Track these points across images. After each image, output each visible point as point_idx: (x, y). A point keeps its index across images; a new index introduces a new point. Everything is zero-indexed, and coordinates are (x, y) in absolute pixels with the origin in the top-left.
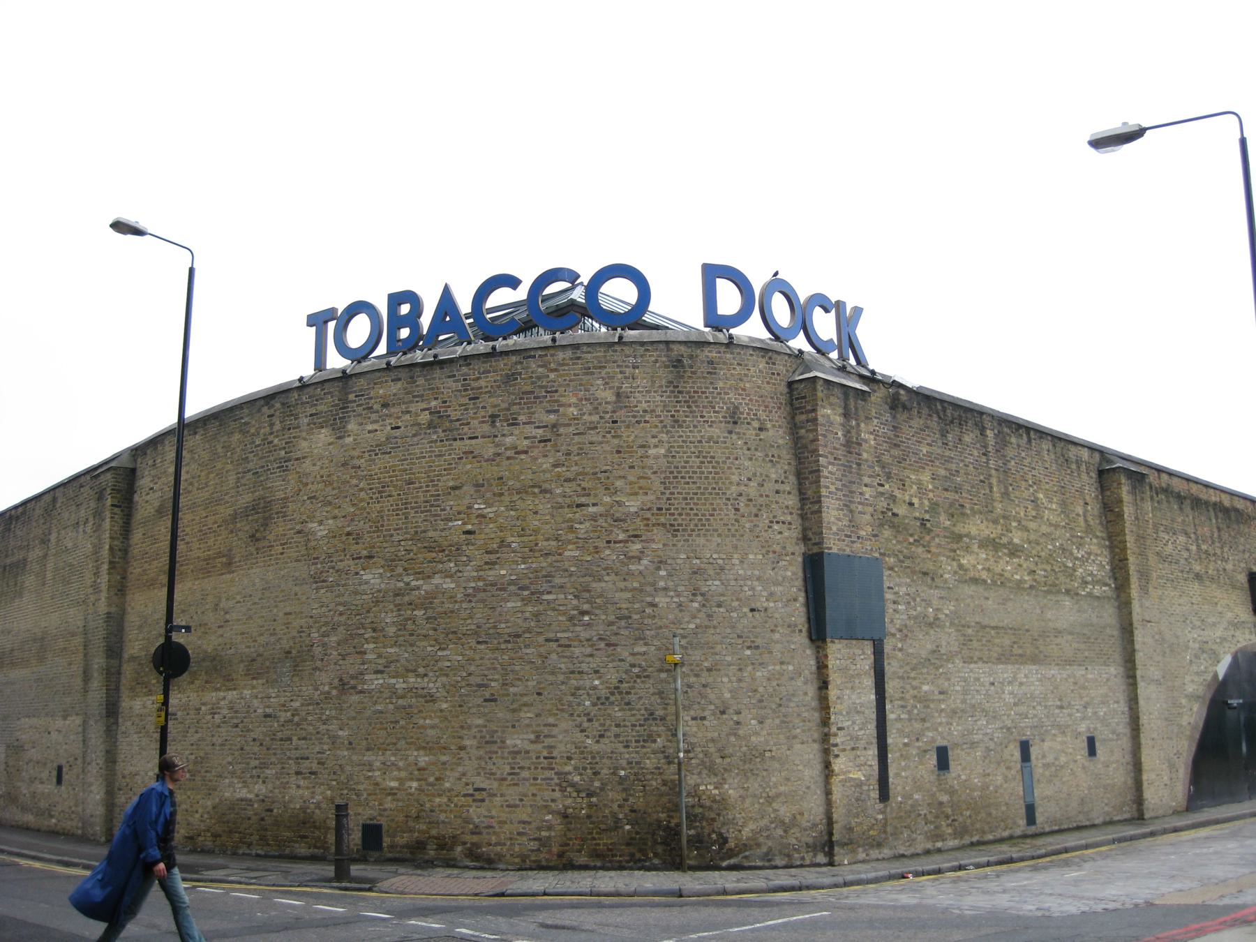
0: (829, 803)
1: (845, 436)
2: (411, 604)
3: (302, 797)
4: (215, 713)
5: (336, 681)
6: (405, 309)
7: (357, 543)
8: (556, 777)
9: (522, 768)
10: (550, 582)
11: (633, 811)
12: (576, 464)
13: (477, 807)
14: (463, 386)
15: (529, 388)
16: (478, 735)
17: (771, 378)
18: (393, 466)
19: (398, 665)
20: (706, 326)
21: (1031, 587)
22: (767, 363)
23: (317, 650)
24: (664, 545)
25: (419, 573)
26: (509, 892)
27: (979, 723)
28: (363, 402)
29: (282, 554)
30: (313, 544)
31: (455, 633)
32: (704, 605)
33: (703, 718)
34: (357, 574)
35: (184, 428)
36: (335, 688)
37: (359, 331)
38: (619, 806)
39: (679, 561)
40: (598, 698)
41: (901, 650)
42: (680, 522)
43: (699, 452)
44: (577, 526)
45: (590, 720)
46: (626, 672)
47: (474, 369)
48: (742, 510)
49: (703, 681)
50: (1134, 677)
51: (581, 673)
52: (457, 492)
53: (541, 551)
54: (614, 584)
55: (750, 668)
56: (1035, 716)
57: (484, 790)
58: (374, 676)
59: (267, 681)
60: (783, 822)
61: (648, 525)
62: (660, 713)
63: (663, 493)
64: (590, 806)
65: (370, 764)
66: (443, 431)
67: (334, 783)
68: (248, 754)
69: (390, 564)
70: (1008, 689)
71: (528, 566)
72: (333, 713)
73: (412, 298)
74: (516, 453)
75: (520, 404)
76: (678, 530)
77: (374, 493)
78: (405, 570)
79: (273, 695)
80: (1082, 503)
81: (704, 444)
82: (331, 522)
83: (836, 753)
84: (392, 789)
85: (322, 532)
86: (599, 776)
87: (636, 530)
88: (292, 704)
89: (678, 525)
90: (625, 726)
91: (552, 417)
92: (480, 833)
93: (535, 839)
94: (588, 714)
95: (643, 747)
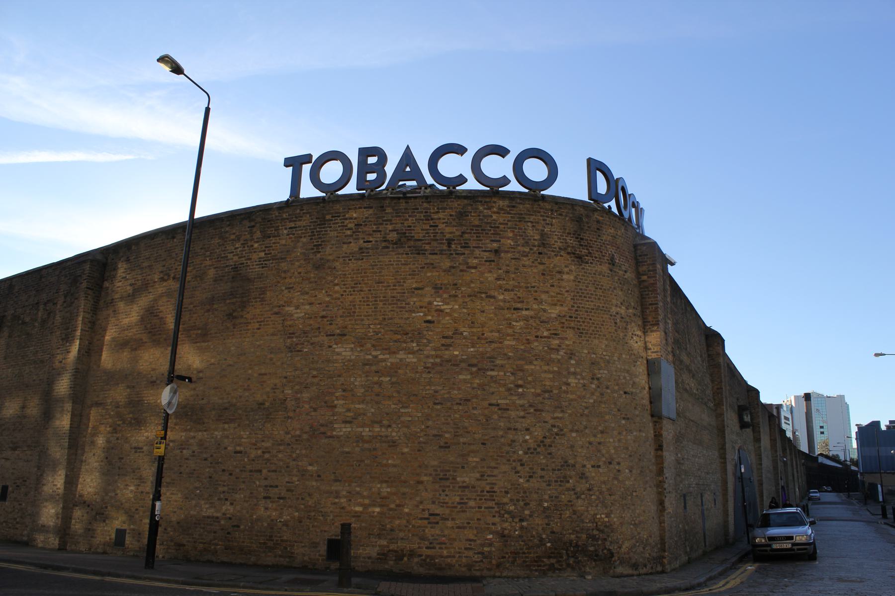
0: (662, 529)
3: (269, 516)
4: (184, 449)
5: (307, 429)
7: (331, 324)
8: (496, 506)
10: (493, 362)
11: (553, 532)
12: (513, 279)
13: (432, 528)
15: (477, 223)
16: (434, 473)
18: (365, 269)
19: (365, 418)
23: (290, 404)
24: (574, 342)
29: (259, 329)
30: (289, 323)
31: (416, 395)
32: (598, 387)
33: (599, 467)
36: (306, 433)
39: (584, 355)
40: (529, 449)
43: (595, 281)
44: (514, 323)
45: (522, 465)
46: (549, 430)
48: (618, 325)
49: (598, 440)
50: (725, 458)
52: (420, 292)
53: (486, 339)
54: (541, 367)
57: (438, 515)
58: (343, 425)
59: (239, 425)
61: (563, 327)
62: (571, 462)
63: (573, 306)
64: (522, 528)
67: (302, 506)
68: (217, 481)
69: (360, 342)
72: (304, 452)
75: (470, 233)
76: (582, 333)
79: (245, 436)
82: (307, 307)
84: (356, 512)
85: (299, 314)
86: (528, 507)
87: (556, 330)
88: (263, 444)
89: (583, 329)
90: (548, 470)
91: (495, 245)
92: (434, 548)
93: (479, 553)
94: (521, 460)
95: (560, 485)
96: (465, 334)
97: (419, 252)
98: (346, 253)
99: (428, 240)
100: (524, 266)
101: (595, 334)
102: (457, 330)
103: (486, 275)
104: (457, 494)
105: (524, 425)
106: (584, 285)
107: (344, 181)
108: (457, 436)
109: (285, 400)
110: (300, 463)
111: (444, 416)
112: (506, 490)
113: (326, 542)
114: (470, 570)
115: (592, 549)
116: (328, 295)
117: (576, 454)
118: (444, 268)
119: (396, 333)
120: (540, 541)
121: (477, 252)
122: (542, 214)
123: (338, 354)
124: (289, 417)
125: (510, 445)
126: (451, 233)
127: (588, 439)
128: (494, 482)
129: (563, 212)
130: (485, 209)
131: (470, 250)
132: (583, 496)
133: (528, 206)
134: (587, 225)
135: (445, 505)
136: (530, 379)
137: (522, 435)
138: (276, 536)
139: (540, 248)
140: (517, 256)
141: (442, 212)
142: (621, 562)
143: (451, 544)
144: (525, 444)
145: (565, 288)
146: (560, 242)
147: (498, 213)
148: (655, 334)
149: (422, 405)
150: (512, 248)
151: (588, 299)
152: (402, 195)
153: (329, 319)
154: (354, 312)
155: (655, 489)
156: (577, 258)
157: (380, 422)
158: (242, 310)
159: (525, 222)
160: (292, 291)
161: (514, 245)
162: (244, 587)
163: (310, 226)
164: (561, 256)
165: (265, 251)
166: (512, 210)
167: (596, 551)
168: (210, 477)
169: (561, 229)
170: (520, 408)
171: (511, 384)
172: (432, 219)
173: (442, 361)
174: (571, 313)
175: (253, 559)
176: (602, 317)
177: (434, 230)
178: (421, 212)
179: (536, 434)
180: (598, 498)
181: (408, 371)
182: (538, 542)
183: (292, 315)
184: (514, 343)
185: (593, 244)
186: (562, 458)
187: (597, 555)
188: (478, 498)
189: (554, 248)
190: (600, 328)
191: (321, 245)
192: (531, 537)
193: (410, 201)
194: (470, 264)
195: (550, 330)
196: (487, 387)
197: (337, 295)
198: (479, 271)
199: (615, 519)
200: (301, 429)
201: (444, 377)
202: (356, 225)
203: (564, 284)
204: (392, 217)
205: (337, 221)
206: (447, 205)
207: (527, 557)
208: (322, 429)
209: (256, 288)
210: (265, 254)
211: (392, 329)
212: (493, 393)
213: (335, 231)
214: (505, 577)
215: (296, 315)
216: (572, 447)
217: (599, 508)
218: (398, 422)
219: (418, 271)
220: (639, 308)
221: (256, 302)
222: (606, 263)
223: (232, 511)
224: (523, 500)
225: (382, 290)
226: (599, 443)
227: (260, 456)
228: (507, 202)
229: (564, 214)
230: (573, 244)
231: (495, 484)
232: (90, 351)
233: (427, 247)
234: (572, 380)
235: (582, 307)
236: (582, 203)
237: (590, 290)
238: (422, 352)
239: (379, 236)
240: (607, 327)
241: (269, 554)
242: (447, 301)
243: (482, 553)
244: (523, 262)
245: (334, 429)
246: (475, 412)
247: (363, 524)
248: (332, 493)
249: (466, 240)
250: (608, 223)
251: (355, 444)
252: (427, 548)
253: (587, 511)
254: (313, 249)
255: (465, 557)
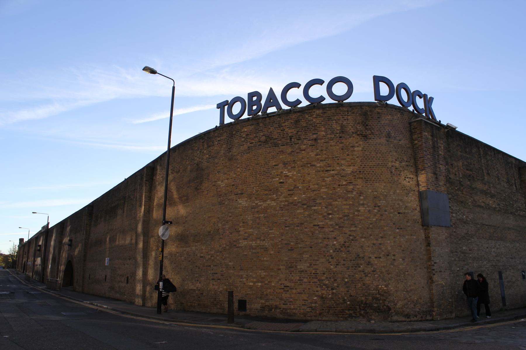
1: (433, 144)
2: (258, 212)
3: (214, 289)
4: (181, 256)
6: (255, 98)
7: (237, 189)
8: (318, 282)
9: (304, 278)
10: (315, 202)
11: (351, 296)
12: (325, 154)
13: (285, 293)
14: (278, 125)
15: (305, 125)
17: (403, 121)
19: (253, 236)
20: (375, 100)
21: (499, 210)
22: (401, 115)
24: (362, 186)
25: (261, 199)
26: (300, 330)
27: (484, 263)
28: (239, 134)
29: (207, 194)
30: (219, 190)
32: (379, 211)
33: (380, 258)
34: (236, 200)
35: (171, 151)
36: (228, 246)
37: (237, 109)
38: (345, 294)
39: (369, 193)
40: (336, 249)
41: (455, 232)
42: (368, 177)
44: (326, 179)
45: (332, 258)
47: (283, 119)
49: (379, 242)
51: (328, 238)
52: (276, 167)
53: (311, 189)
54: (342, 202)
55: (398, 237)
56: (503, 261)
57: (288, 286)
58: (243, 241)
59: (201, 244)
60: (413, 302)
61: (355, 178)
63: (361, 165)
64: (333, 293)
65: (242, 276)
66: (271, 143)
67: (227, 283)
70: (493, 250)
71: (306, 195)
73: (258, 95)
74: (300, 151)
75: (301, 131)
76: (368, 180)
77: (243, 169)
78: (256, 198)
79: (204, 249)
80: (514, 179)
81: (377, 146)
82: (226, 181)
83: (434, 273)
84: (250, 286)
86: (336, 281)
87: (351, 180)
88: (211, 252)
90: (347, 260)
91: (315, 136)
92: (287, 304)
94: (332, 256)
95: (355, 269)
96: (300, 187)
97: (276, 145)
98: (242, 151)
99: (280, 138)
100: (331, 146)
101: (376, 180)
102: (295, 186)
103: (310, 153)
104: (298, 275)
105: (333, 236)
106: (369, 152)
107: (242, 113)
108: (297, 244)
109: (219, 229)
110: (226, 261)
111: (290, 233)
112: (324, 272)
113: (238, 302)
114: (305, 316)
115: (376, 305)
116: (235, 174)
117: (364, 251)
118: (288, 152)
119: (266, 190)
120: (343, 301)
121: (305, 141)
122: (342, 114)
123: (240, 204)
124: (221, 238)
125: (325, 247)
126: (291, 133)
127: (372, 242)
128: (317, 268)
129: (355, 111)
130: (309, 116)
131: (302, 141)
132: (369, 275)
133: (333, 111)
134: (370, 116)
135: (292, 281)
136: (336, 209)
137: (332, 241)
138: (217, 299)
139: (340, 134)
140: (327, 140)
141: (287, 122)
142: (396, 313)
143: (295, 302)
144: (334, 246)
145: (355, 155)
146: (353, 129)
147: (316, 118)
148: (423, 175)
149: (279, 228)
150: (324, 136)
151: (371, 160)
152: (266, 116)
153: (236, 186)
154: (247, 181)
155: (426, 270)
156: (364, 137)
157: (259, 238)
158: (201, 186)
159: (331, 120)
160: (220, 173)
161: (325, 135)
162: (186, 322)
163: (226, 138)
164: (353, 137)
165: (208, 154)
166: (324, 115)
167: (378, 306)
168: (192, 270)
169: (353, 121)
170: (330, 226)
171: (325, 213)
172: (282, 126)
173: (289, 203)
174: (360, 170)
175: (209, 310)
176: (381, 170)
177: (283, 132)
178: (277, 123)
179: (340, 240)
180: (380, 276)
181: (272, 211)
182: (342, 301)
183: (220, 186)
184: (326, 190)
185: (375, 127)
186: (356, 253)
187: (379, 309)
188: (308, 277)
189: (349, 133)
190: (380, 176)
191: (231, 148)
192: (338, 298)
193: (271, 118)
194: (302, 149)
195: (347, 181)
196: (312, 216)
197: (239, 173)
198: (306, 152)
199: (391, 288)
200: (226, 244)
201: (290, 212)
202: (246, 135)
203: (355, 153)
204: (263, 128)
205: (238, 134)
206: (289, 117)
207: (336, 310)
208: (235, 243)
209: (206, 173)
210: (209, 156)
211: (264, 188)
212: (315, 219)
213: (237, 139)
214: (324, 321)
215: (222, 186)
216: (362, 247)
217: (380, 282)
218: (268, 238)
219: (276, 156)
220: (412, 161)
221: (206, 180)
222: (384, 137)
223: (200, 286)
224: (333, 278)
225: (258, 168)
226: (380, 244)
227: (210, 259)
228: (321, 111)
229: (355, 112)
230: (361, 129)
231: (317, 269)
232: (149, 211)
233: (280, 142)
234: (361, 209)
235: (367, 165)
236: (369, 104)
237: (373, 155)
238: (278, 200)
239: (257, 139)
240: (385, 175)
241: (215, 307)
242: (290, 170)
243: (311, 307)
244: (331, 144)
245: (239, 243)
246: (306, 230)
247: (254, 292)
248: (239, 276)
249: (299, 135)
250: (386, 113)
251: (249, 251)
252: (283, 304)
253: (372, 283)
254: (228, 150)
255: (302, 309)
